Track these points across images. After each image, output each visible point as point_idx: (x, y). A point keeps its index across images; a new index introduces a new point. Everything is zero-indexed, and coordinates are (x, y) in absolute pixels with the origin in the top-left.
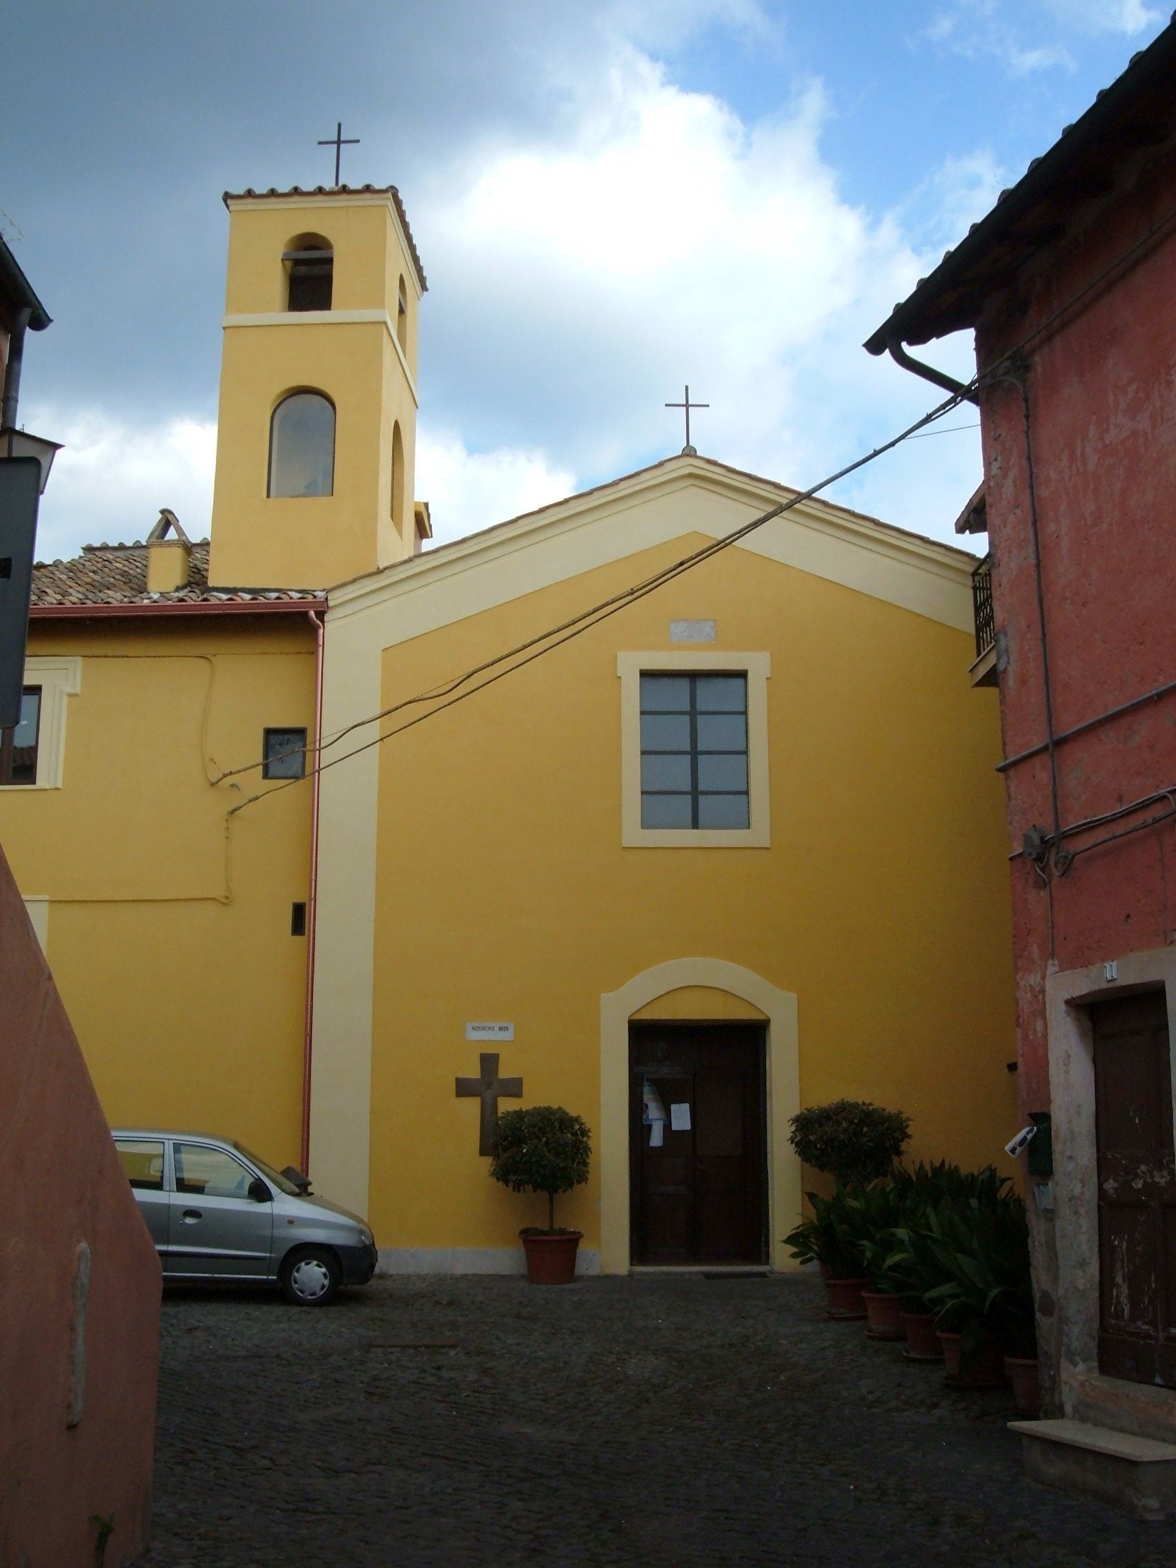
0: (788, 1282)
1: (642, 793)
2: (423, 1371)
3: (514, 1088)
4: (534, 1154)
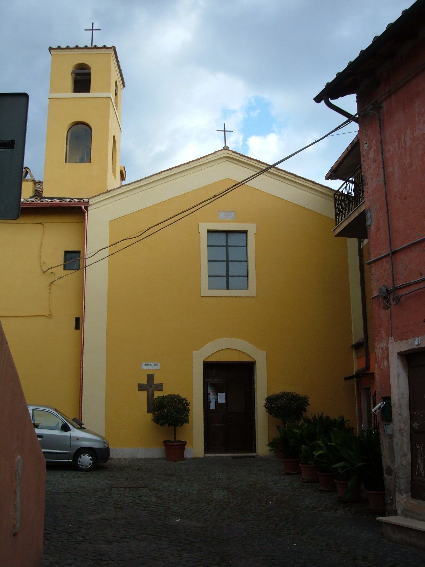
0: (264, 459)
1: (208, 276)
2: (135, 498)
3: (160, 387)
4: (168, 412)
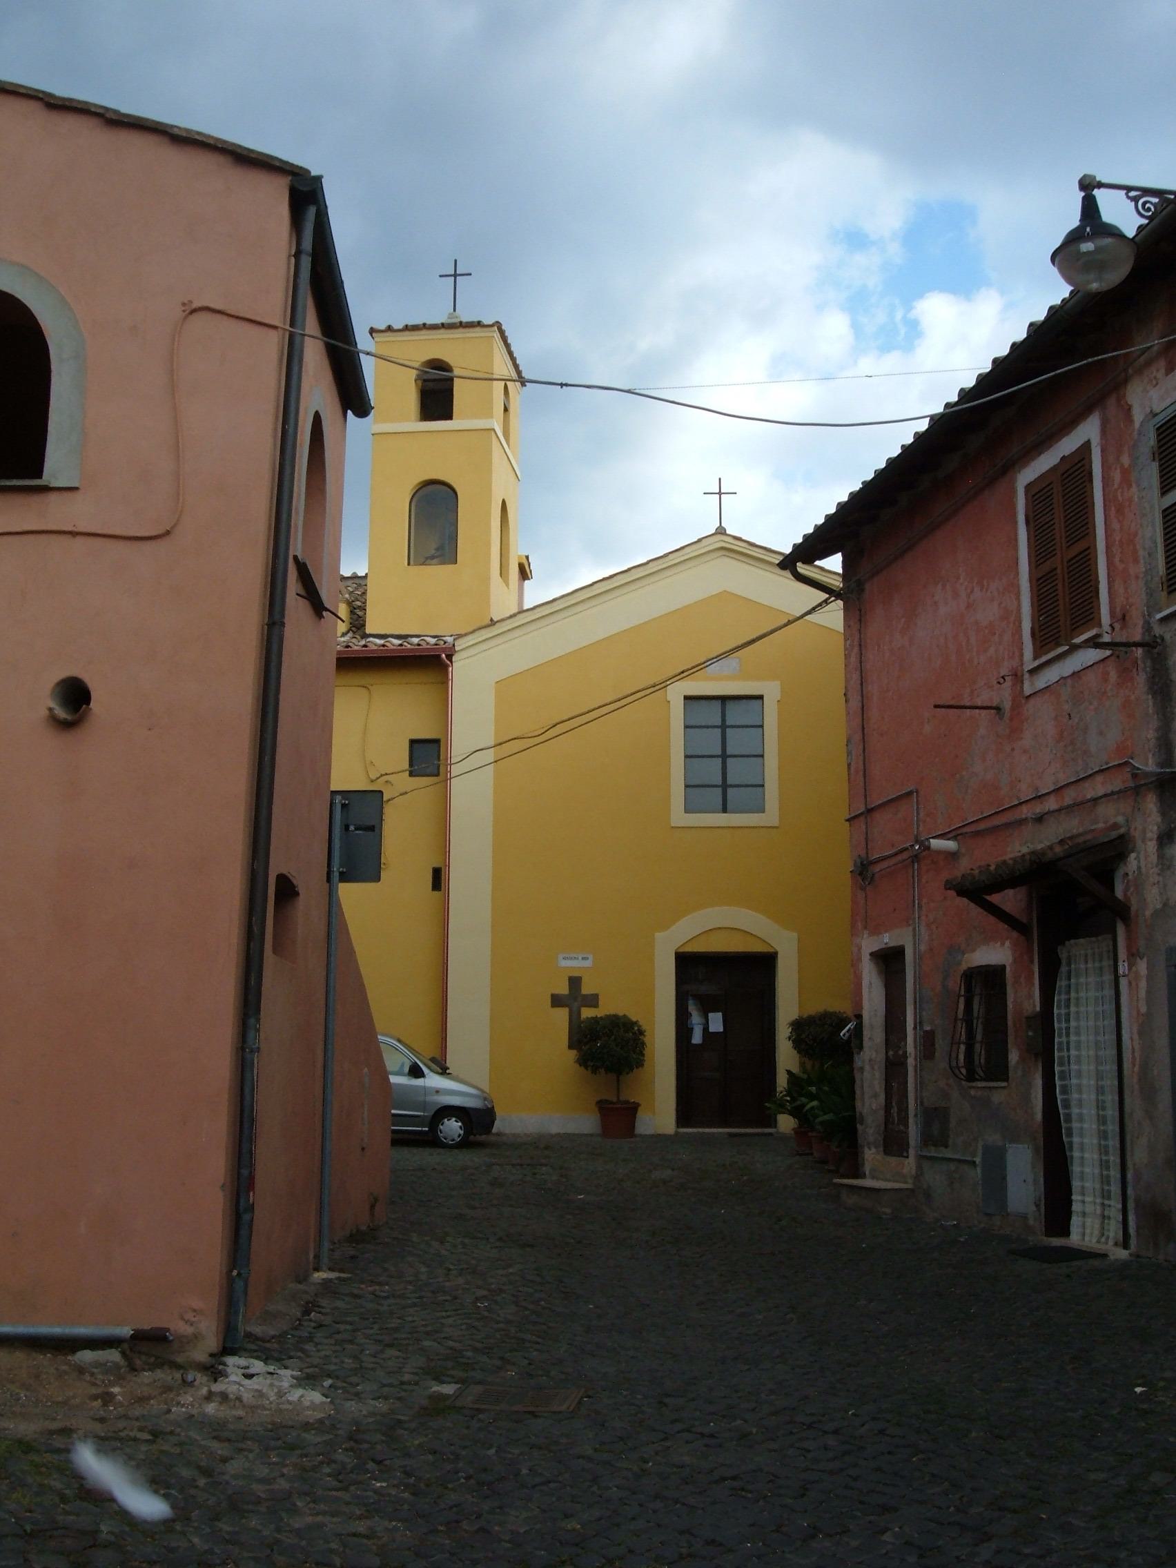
0: (783, 1138)
3: (593, 1001)
4: (606, 1047)
